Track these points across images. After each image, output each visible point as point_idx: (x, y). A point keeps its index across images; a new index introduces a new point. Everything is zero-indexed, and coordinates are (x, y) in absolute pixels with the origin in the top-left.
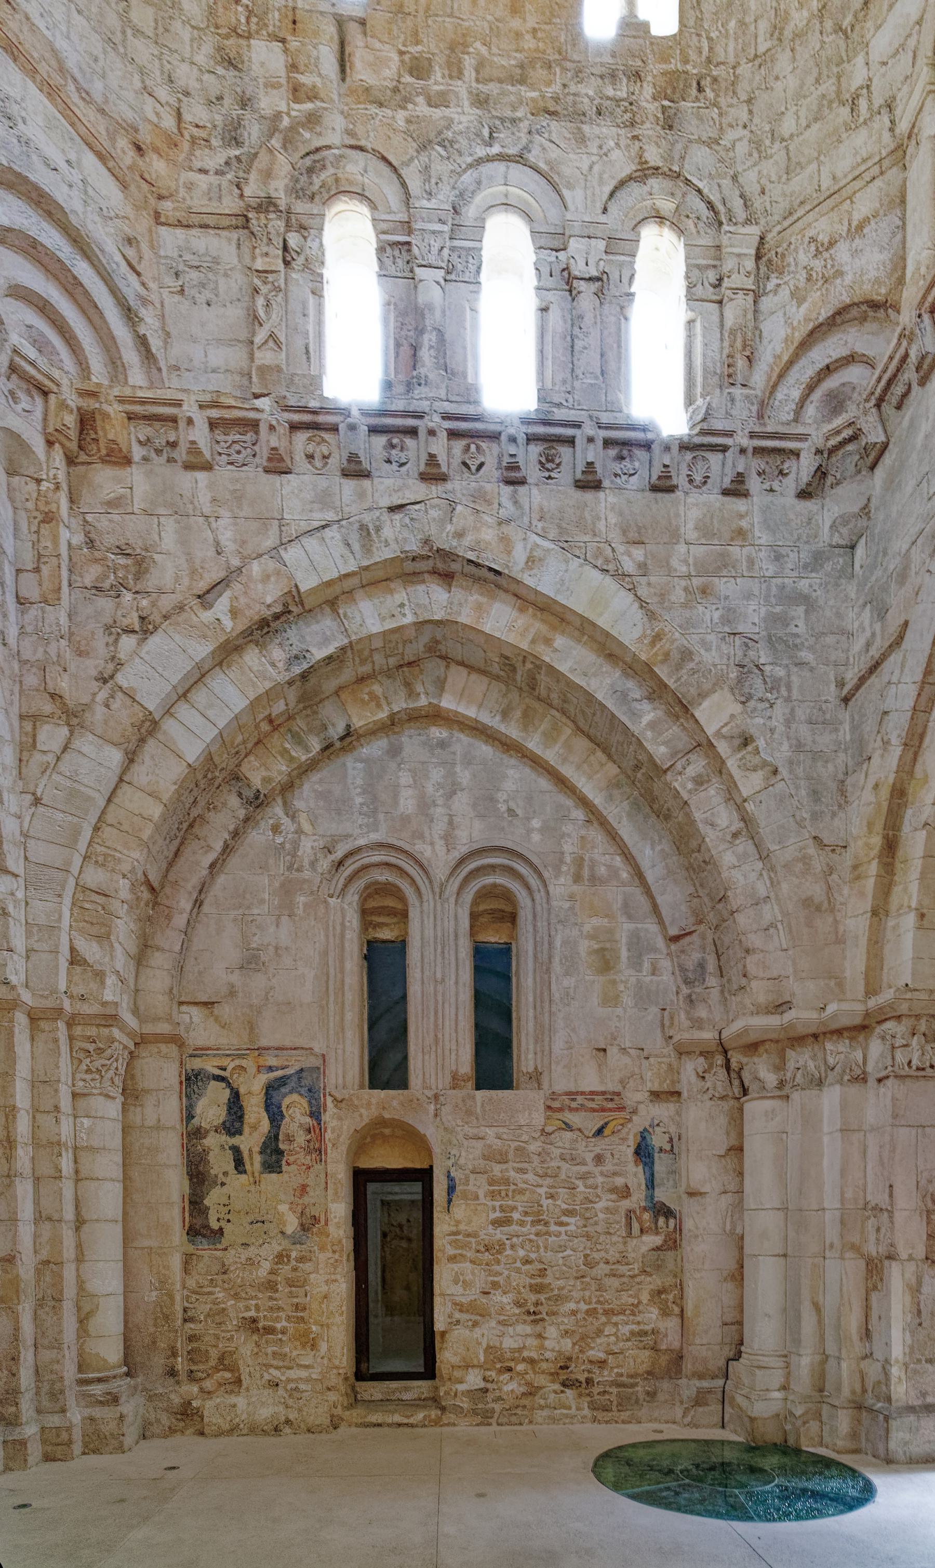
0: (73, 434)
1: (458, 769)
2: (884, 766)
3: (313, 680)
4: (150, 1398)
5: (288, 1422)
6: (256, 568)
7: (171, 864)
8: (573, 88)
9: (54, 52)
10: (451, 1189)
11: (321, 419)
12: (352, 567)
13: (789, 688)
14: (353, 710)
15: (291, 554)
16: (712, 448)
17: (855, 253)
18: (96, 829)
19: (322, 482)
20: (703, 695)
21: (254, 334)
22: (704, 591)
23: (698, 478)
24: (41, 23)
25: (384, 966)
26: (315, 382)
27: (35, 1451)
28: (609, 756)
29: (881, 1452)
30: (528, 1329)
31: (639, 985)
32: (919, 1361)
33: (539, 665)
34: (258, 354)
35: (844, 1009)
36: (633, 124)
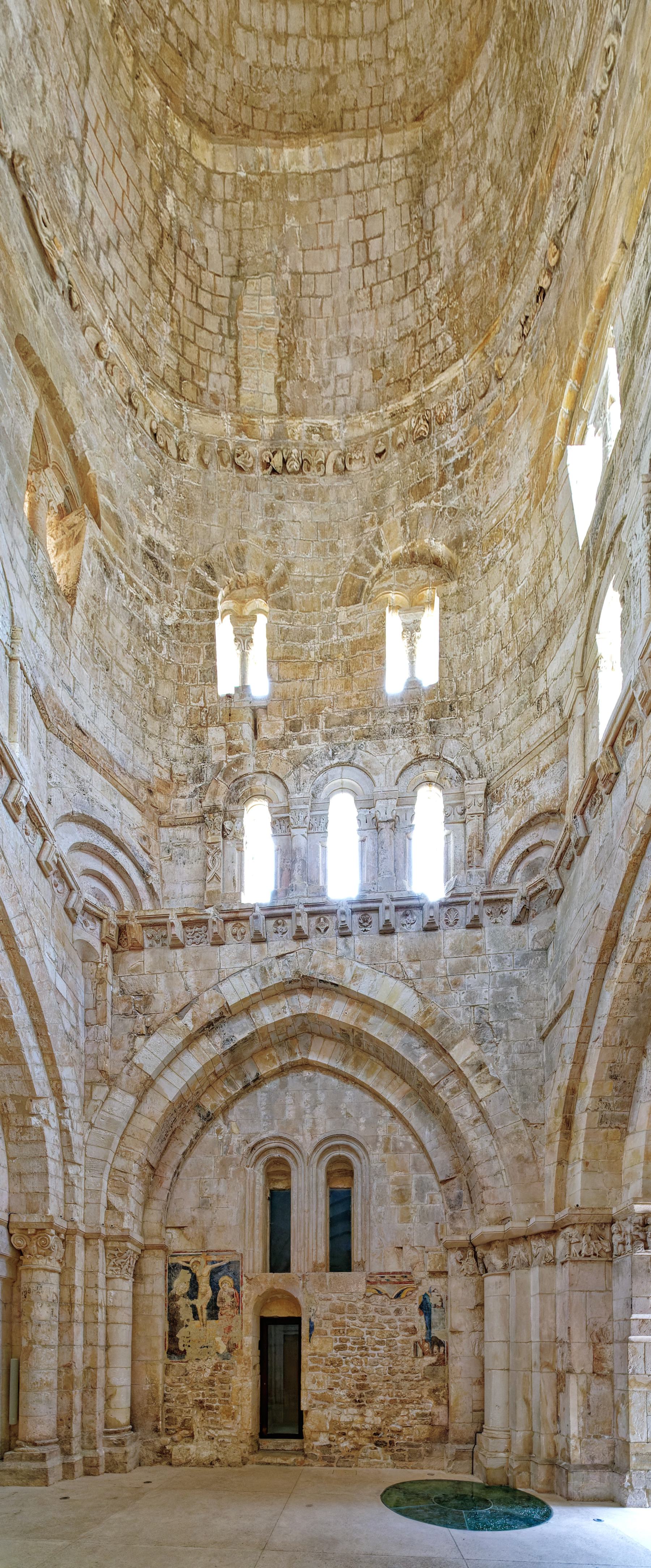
0: (115, 938)
2: (562, 1077)
3: (237, 1052)
4: (144, 1444)
5: (218, 1460)
6: (205, 995)
7: (162, 1155)
8: (378, 722)
9: (108, 753)
10: (311, 1329)
11: (240, 915)
12: (257, 990)
13: (507, 1033)
14: (260, 1066)
15: (225, 987)
16: (459, 904)
17: (541, 785)
18: (122, 1138)
19: (241, 947)
20: (454, 1043)
21: (206, 875)
22: (456, 984)
23: (451, 921)
24: (102, 742)
25: (279, 1203)
26: (237, 896)
27: (79, 1469)
28: (404, 1080)
29: (564, 1493)
30: (355, 1411)
31: (423, 1210)
32: (589, 1437)
33: (361, 1033)
34: (208, 886)
35: (542, 1222)
36: (413, 734)
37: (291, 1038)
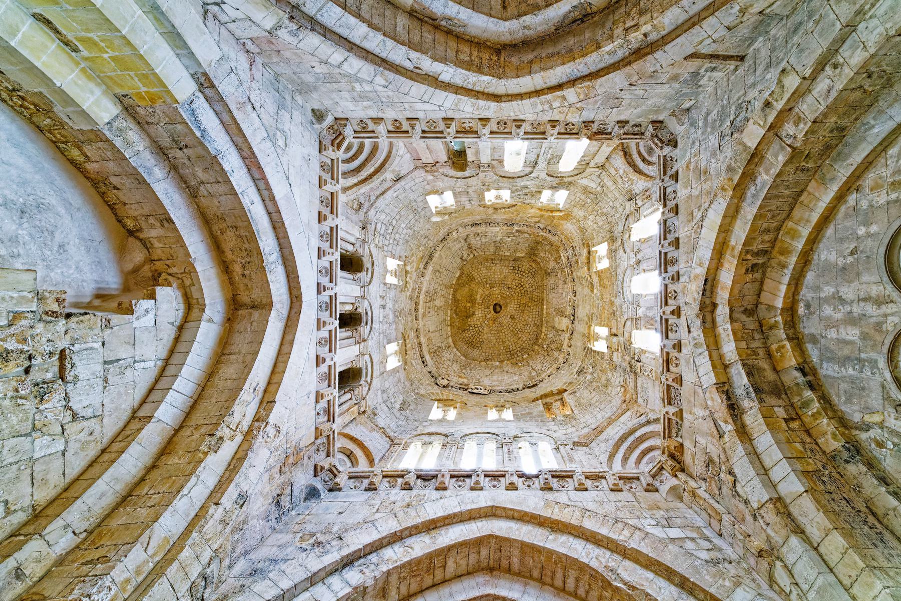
0: (675, 464)
1: (823, 295)
12: (706, 354)
28: (803, 191)
37: (761, 326)
